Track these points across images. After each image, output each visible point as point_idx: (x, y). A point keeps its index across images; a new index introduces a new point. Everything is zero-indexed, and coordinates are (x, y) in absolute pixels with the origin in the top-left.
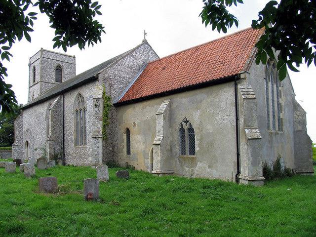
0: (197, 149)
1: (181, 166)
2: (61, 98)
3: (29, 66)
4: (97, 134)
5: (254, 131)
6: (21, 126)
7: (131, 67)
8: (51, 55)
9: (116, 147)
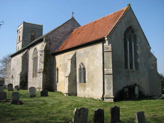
0: (87, 80)
1: (80, 89)
2: (27, 50)
3: (18, 32)
4: (40, 71)
5: (109, 70)
6: (10, 66)
7: (63, 33)
8: (29, 25)
9: (52, 79)
